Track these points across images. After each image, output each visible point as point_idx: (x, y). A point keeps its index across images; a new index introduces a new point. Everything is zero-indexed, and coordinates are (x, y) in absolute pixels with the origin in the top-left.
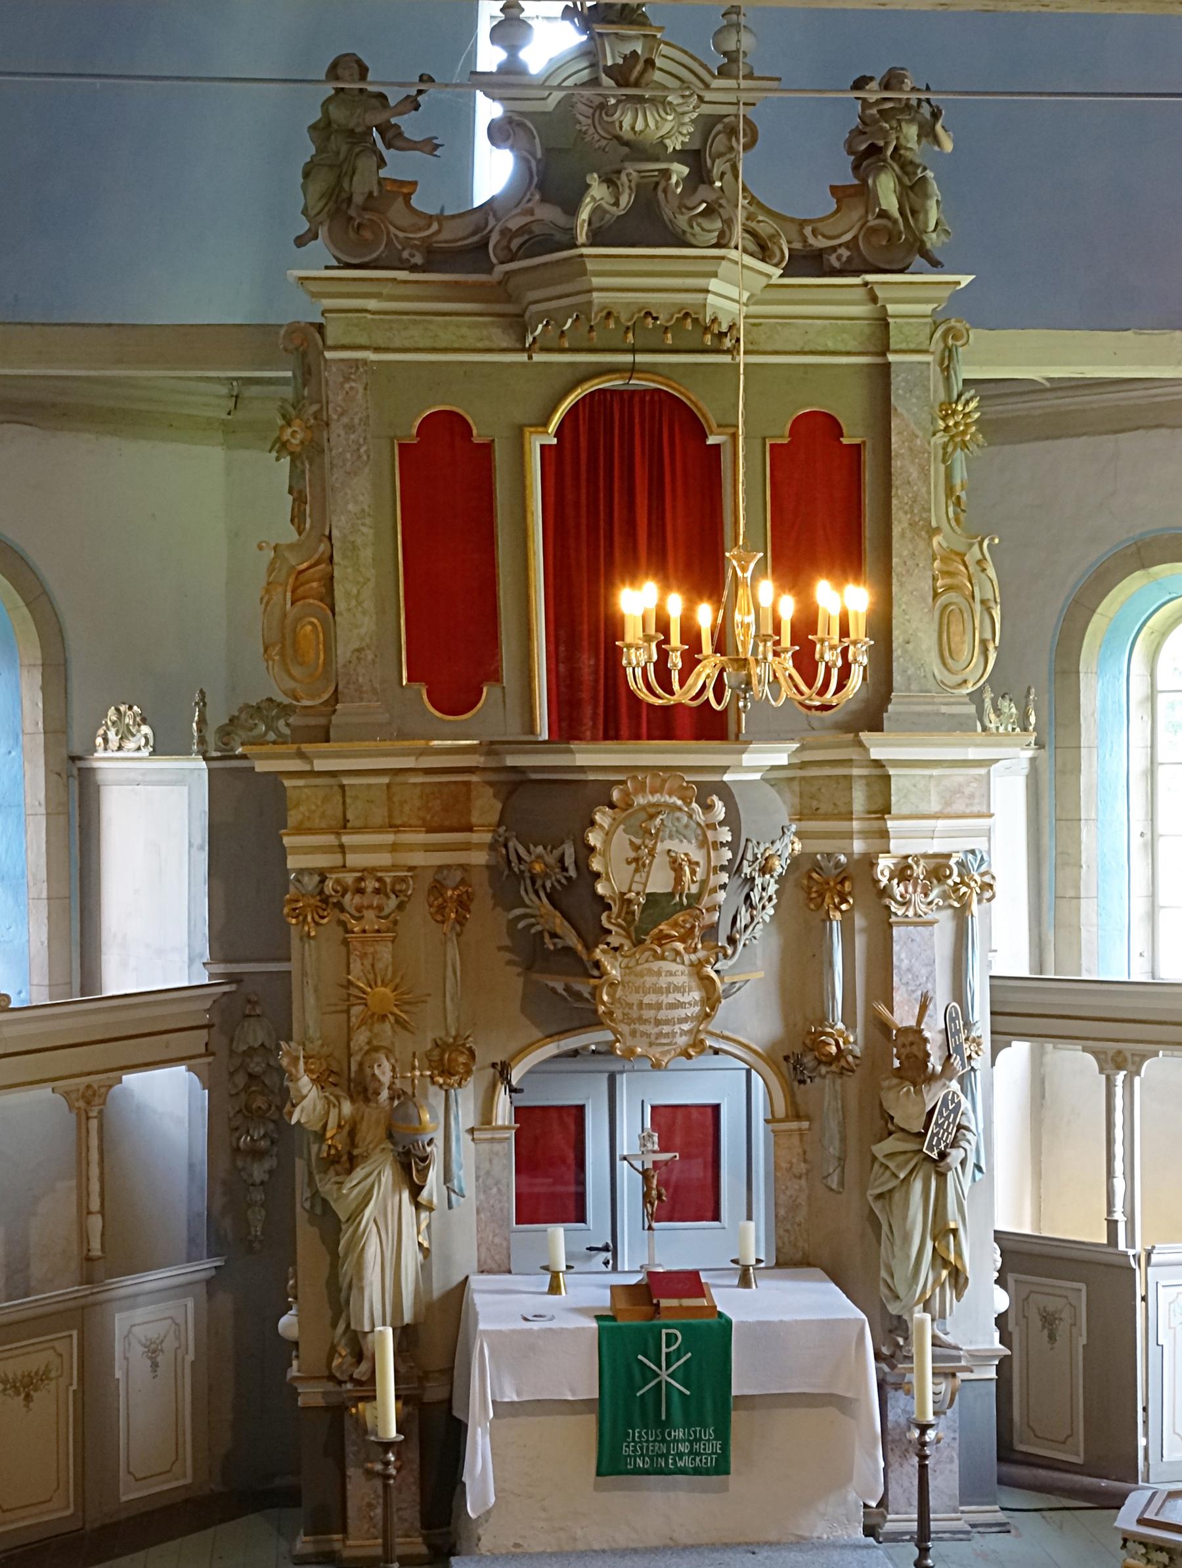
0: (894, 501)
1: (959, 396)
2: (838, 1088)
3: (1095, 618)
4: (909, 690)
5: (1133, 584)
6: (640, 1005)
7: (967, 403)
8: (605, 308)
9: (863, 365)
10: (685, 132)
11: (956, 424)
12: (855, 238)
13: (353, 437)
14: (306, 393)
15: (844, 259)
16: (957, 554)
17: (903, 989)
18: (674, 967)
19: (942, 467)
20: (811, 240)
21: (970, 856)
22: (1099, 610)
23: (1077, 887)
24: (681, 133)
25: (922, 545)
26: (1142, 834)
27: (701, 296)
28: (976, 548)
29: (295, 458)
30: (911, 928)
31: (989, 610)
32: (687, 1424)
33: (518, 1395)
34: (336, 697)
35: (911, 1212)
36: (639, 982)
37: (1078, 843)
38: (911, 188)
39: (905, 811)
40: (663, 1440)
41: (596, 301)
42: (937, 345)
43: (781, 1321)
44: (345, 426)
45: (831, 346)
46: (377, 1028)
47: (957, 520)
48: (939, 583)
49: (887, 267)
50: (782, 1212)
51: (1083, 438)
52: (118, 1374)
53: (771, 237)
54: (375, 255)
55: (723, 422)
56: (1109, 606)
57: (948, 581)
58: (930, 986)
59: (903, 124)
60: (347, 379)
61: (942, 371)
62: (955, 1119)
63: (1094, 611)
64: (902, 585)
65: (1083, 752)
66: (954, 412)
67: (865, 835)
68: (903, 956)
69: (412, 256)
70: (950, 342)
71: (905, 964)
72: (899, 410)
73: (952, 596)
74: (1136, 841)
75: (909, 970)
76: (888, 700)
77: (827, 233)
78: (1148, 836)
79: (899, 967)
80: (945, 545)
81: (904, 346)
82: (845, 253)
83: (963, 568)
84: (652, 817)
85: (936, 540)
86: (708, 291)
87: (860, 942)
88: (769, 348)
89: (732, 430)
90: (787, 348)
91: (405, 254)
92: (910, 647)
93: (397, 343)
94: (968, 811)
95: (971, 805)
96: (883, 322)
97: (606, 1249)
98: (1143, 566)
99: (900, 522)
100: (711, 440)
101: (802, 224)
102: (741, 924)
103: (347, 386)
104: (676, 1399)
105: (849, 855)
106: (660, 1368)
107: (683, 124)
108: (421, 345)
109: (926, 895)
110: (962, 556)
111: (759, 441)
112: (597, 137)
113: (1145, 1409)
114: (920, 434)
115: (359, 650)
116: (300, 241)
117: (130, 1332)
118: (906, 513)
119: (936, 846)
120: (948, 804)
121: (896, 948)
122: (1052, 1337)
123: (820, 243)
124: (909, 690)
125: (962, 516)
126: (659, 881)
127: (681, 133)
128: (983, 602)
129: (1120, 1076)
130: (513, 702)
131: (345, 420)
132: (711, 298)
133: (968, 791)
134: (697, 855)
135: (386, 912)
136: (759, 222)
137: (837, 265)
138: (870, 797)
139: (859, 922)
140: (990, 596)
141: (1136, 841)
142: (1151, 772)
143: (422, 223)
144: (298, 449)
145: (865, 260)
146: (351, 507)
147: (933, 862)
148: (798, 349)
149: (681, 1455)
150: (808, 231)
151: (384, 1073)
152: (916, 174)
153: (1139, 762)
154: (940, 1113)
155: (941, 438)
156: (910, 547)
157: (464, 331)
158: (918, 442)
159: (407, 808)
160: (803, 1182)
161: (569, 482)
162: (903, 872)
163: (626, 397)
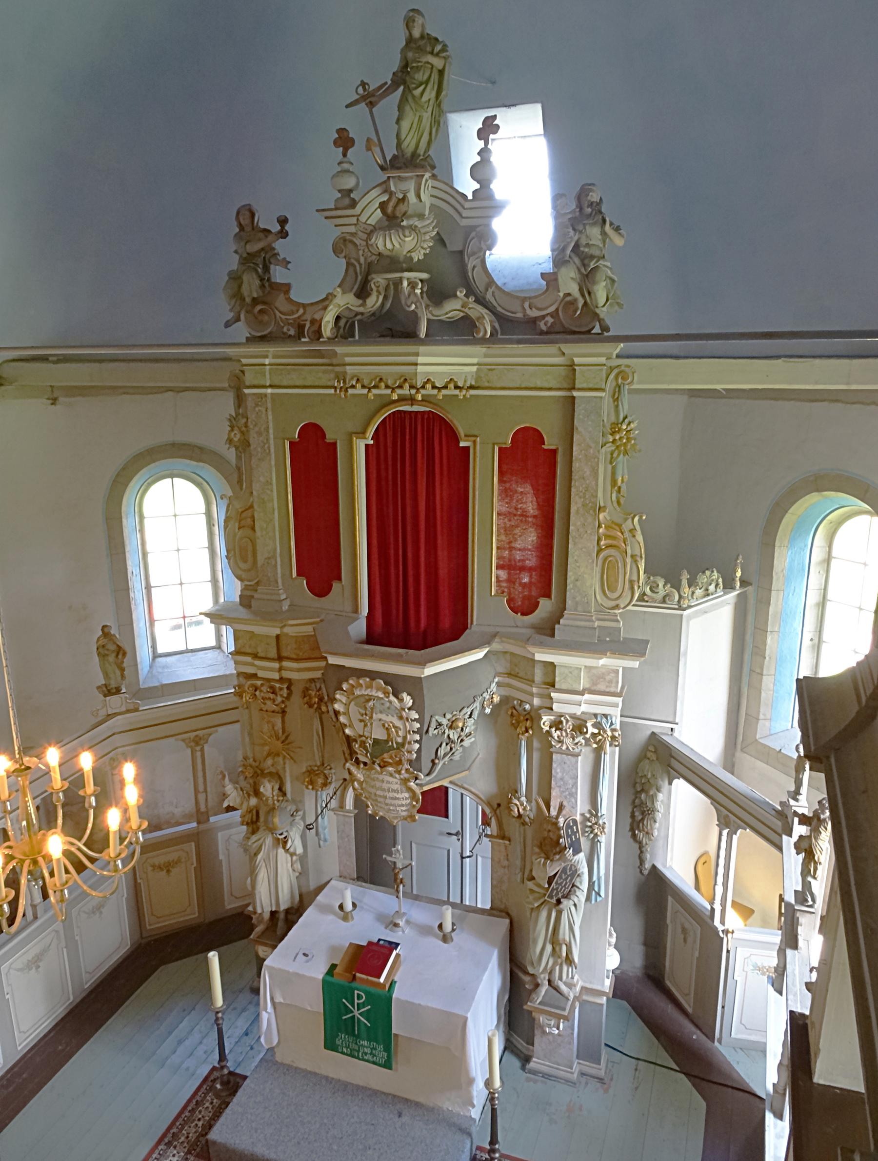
0: (573, 490)
1: (625, 418)
2: (522, 832)
3: (787, 516)
4: (576, 610)
5: (813, 498)
6: (375, 794)
7: (629, 423)
8: (355, 376)
9: (560, 397)
10: (425, 246)
11: (621, 438)
12: (557, 310)
13: (261, 439)
14: (241, 411)
15: (549, 324)
16: (616, 524)
17: (557, 789)
18: (391, 779)
19: (610, 467)
20: (528, 312)
21: (604, 720)
22: (790, 511)
23: (762, 668)
24: (422, 248)
25: (590, 520)
26: (812, 640)
27: (413, 367)
28: (630, 520)
29: (237, 448)
30: (564, 756)
31: (636, 561)
32: (369, 1040)
33: (284, 999)
34: (258, 583)
35: (538, 928)
36: (373, 783)
37: (765, 644)
38: (587, 276)
39: (564, 687)
40: (356, 1044)
41: (348, 372)
42: (610, 385)
43: (419, 1005)
44: (257, 432)
45: (539, 384)
46: (276, 759)
47: (618, 503)
48: (602, 543)
49: (577, 329)
50: (495, 883)
51: (792, 402)
52: (221, 857)
53: (478, 318)
54: (269, 330)
55: (468, 433)
56: (789, 519)
57: (609, 542)
58: (574, 790)
59: (587, 227)
60: (257, 405)
61: (614, 401)
62: (571, 880)
63: (787, 512)
64: (575, 544)
65: (773, 593)
66: (620, 430)
67: (541, 696)
68: (558, 770)
69: (289, 330)
70: (620, 381)
71: (559, 775)
72: (580, 429)
73: (611, 551)
74: (806, 642)
75: (562, 779)
76: (561, 616)
77: (539, 306)
78: (816, 641)
79: (555, 777)
80: (608, 518)
81: (585, 385)
82: (550, 320)
83: (620, 534)
84: (368, 701)
85: (601, 516)
86: (416, 364)
87: (536, 756)
88: (499, 385)
89: (473, 439)
90: (511, 385)
91: (285, 330)
92: (578, 583)
93: (285, 383)
94: (607, 690)
95: (610, 687)
96: (572, 366)
97: (457, 834)
98: (818, 490)
99: (576, 503)
100: (462, 444)
101: (524, 299)
102: (441, 752)
103: (257, 409)
104: (363, 1027)
105: (532, 705)
106: (354, 1007)
107: (425, 241)
108: (298, 384)
109: (574, 740)
110: (620, 526)
111: (490, 446)
112: (369, 254)
113: (723, 1007)
114: (593, 445)
115: (269, 558)
116: (228, 325)
117: (229, 838)
118: (580, 497)
119: (578, 711)
120: (595, 684)
121: (554, 765)
122: (685, 940)
123: (534, 313)
124: (576, 610)
125: (622, 501)
126: (379, 734)
127: (422, 248)
128: (632, 556)
129: (725, 832)
130: (348, 593)
131: (257, 429)
132: (420, 369)
133: (608, 678)
134: (398, 723)
135: (276, 703)
136: (470, 308)
137: (544, 328)
138: (545, 674)
139: (536, 744)
140: (637, 552)
141: (806, 642)
142: (822, 604)
143: (294, 308)
144: (238, 444)
145: (563, 326)
146: (261, 479)
147: (579, 722)
148: (518, 386)
149: (366, 1054)
150: (526, 305)
151: (266, 790)
152: (589, 266)
153: (813, 598)
154: (560, 877)
155: (610, 447)
156: (582, 519)
157: (320, 374)
158: (592, 451)
159: (289, 648)
160: (506, 870)
161: (383, 467)
162: (557, 724)
163: (413, 416)
